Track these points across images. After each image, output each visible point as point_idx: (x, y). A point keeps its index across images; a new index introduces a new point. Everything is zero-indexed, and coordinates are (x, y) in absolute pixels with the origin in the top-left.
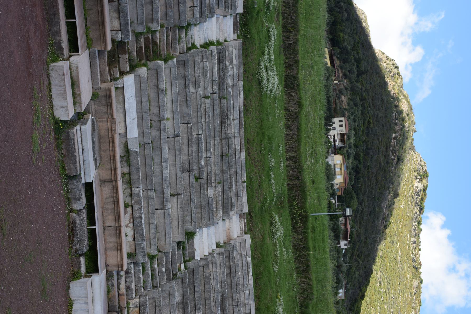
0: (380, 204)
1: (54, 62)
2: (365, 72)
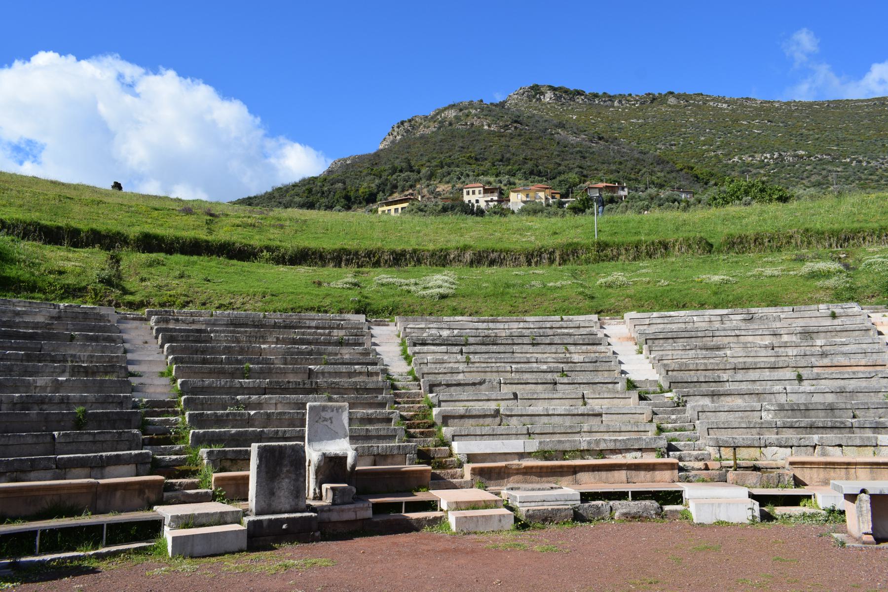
0: (572, 145)
1: (449, 527)
2: (408, 161)
